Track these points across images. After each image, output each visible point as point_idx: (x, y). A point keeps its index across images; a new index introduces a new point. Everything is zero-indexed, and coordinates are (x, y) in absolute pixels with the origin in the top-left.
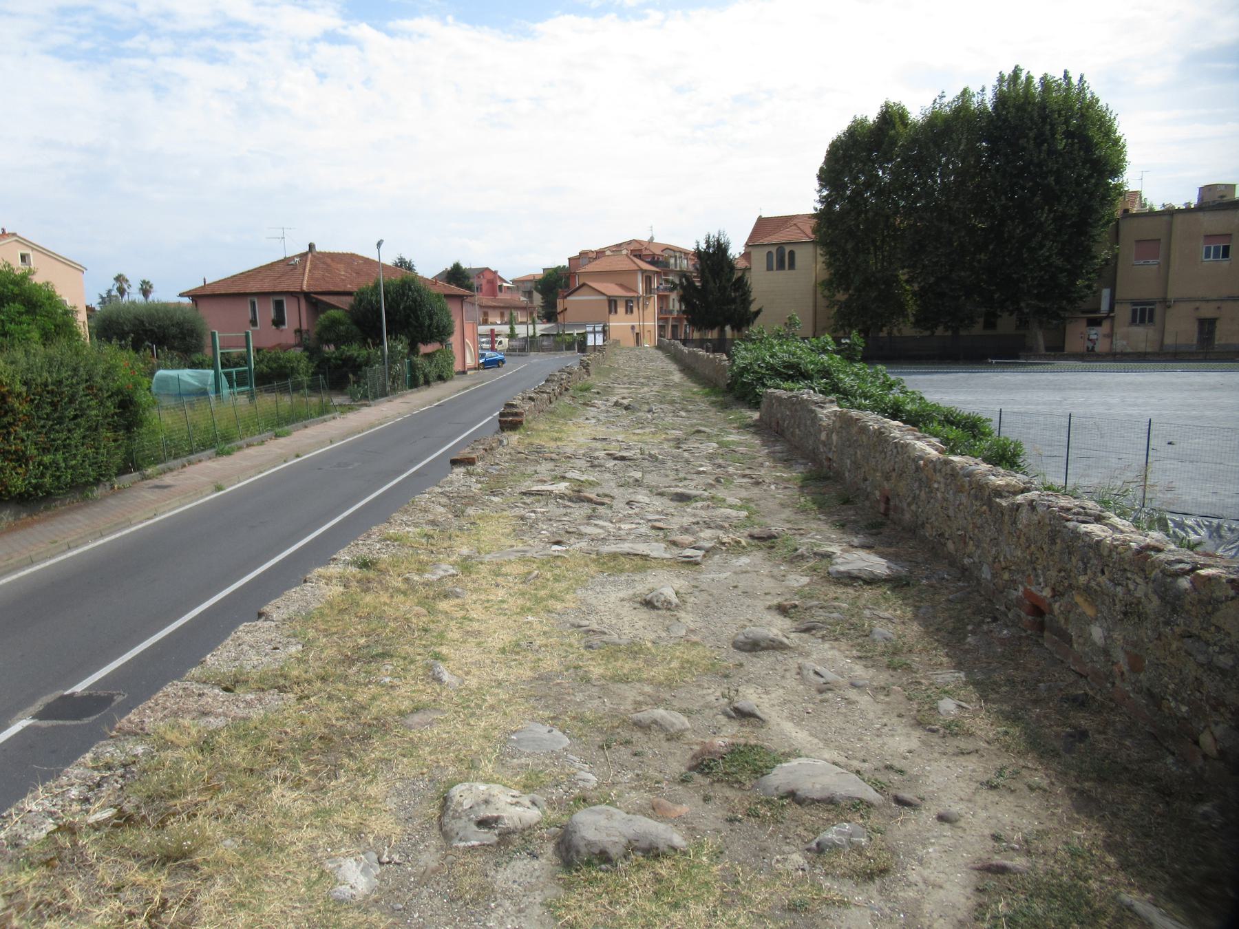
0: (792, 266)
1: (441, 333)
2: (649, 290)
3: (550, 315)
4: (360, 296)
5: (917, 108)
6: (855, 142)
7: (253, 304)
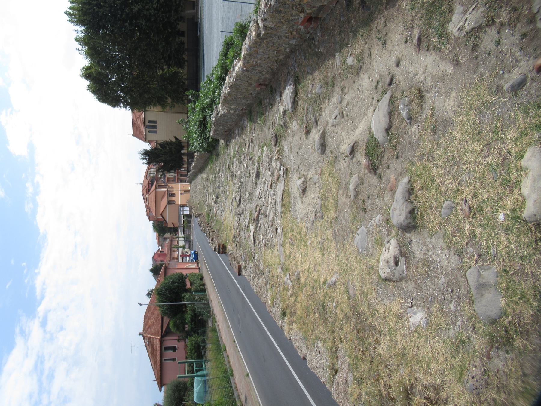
0: (155, 122)
1: (181, 278)
2: (164, 186)
3: (175, 230)
4: (164, 313)
5: (85, 62)
6: (99, 90)
7: (165, 360)
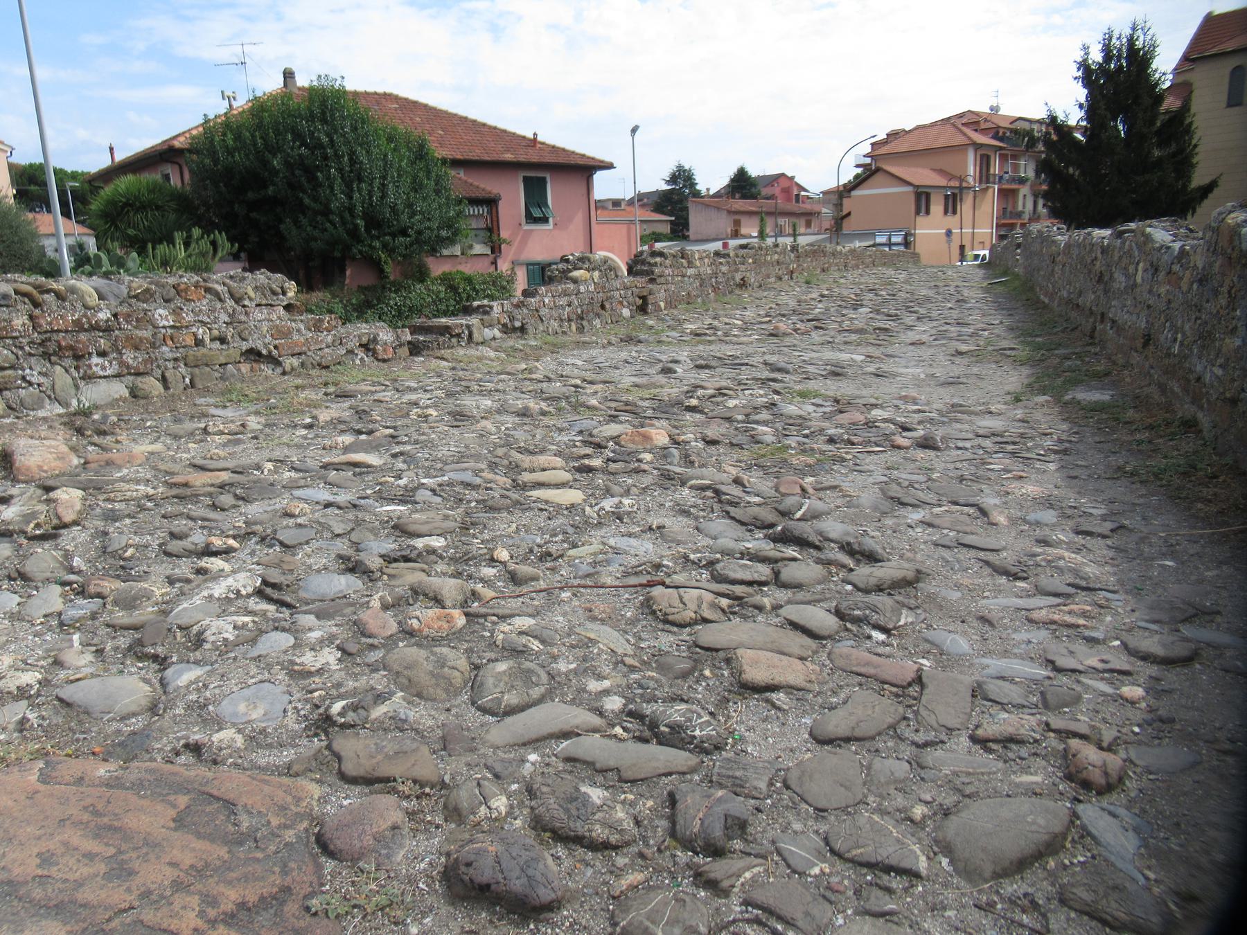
2: (985, 176)
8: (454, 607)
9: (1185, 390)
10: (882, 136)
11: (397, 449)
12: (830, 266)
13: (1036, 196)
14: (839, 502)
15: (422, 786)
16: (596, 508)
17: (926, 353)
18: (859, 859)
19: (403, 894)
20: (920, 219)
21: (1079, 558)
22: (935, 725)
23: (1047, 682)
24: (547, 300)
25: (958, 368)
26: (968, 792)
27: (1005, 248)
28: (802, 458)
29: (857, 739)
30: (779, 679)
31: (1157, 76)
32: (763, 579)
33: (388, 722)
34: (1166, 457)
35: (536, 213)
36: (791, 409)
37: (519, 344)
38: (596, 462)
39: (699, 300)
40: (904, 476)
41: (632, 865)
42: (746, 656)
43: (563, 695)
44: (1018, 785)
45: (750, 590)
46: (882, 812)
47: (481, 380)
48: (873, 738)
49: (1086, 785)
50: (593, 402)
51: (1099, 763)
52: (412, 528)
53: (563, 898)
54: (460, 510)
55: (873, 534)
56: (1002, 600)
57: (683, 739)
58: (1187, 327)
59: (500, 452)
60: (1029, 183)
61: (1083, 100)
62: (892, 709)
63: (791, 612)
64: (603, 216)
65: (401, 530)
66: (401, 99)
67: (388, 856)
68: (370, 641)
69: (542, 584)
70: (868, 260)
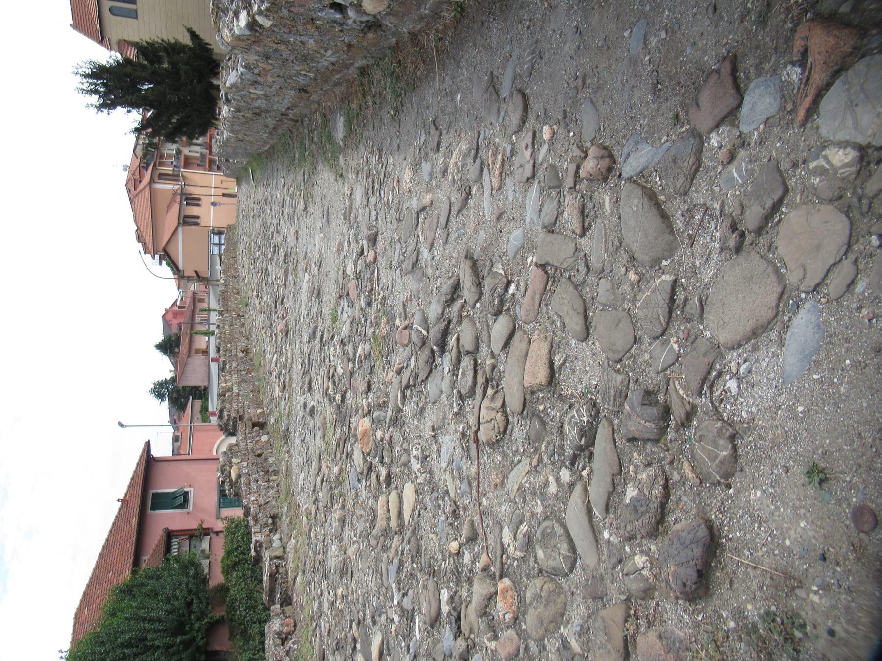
8: (496, 585)
9: (339, 72)
10: (140, 246)
11: (369, 621)
12: (234, 288)
13: (191, 144)
14: (415, 303)
15: (629, 616)
16: (419, 474)
17: (304, 231)
18: (667, 317)
19: (707, 632)
20: (202, 224)
21: (456, 152)
22: (574, 259)
23: (542, 184)
24: (253, 498)
25: (316, 210)
26: (618, 244)
27: (228, 168)
28: (382, 325)
29: (585, 311)
30: (545, 359)
31: (111, 61)
32: (472, 362)
33: (583, 639)
34: (385, 89)
35: (180, 500)
36: (345, 330)
37: (285, 520)
38: (383, 471)
39: (257, 383)
40: (396, 258)
41: (679, 470)
42: (529, 381)
43: (559, 510)
44: (612, 212)
45: (480, 373)
46: (634, 300)
47: (315, 552)
48: (584, 301)
49: (610, 170)
50: (336, 469)
51: (596, 160)
52: (433, 613)
53: (703, 518)
54: (419, 575)
55: (438, 284)
56: (485, 205)
57: (590, 429)
58: (297, 68)
59: (373, 542)
60: (181, 148)
61: (125, 110)
62: (564, 286)
63: (497, 347)
64: (185, 450)
65: (435, 621)
66: (80, 606)
67: (681, 642)
68: (522, 651)
69: (477, 518)
70: (232, 261)
